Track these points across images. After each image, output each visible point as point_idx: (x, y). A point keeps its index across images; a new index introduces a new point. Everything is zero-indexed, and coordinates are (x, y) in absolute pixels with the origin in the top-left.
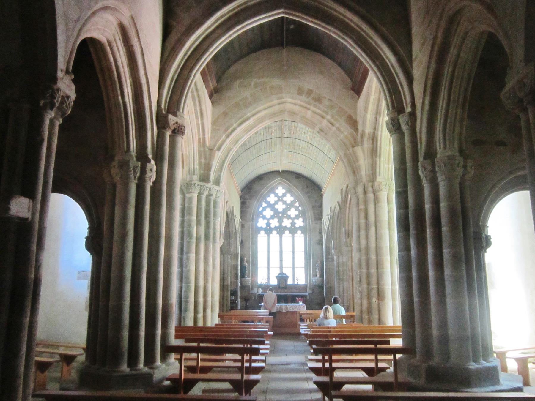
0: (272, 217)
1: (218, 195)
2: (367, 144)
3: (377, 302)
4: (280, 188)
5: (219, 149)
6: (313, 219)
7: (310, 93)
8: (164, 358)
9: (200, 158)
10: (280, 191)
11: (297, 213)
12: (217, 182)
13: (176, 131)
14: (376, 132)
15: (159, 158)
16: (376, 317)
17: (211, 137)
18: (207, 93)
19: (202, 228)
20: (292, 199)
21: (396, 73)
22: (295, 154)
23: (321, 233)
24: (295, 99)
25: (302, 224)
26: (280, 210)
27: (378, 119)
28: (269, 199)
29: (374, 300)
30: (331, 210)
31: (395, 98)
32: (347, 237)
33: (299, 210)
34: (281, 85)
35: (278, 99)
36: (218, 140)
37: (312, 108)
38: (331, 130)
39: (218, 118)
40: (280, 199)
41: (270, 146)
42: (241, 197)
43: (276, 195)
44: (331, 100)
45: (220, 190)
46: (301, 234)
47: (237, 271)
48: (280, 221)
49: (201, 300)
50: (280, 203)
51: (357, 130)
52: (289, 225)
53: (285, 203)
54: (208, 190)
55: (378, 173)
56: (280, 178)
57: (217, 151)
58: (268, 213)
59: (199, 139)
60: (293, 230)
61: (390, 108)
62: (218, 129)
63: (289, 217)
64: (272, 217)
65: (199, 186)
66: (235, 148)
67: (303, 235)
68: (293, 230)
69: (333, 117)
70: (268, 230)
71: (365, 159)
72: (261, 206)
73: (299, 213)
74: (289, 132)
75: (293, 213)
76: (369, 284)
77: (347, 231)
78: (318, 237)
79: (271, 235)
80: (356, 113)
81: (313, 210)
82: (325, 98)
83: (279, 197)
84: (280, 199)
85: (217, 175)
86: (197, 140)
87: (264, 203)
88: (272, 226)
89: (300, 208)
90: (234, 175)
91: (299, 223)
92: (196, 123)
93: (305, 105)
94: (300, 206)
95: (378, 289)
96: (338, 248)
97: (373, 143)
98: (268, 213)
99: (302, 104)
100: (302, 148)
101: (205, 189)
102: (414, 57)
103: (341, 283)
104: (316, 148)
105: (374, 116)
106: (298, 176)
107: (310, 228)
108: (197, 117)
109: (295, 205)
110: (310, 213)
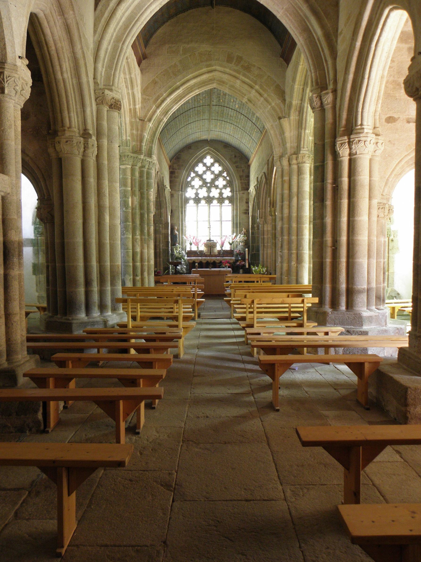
0: (201, 187)
1: (151, 166)
2: (294, 116)
3: (295, 265)
4: (208, 157)
5: (150, 120)
6: (240, 189)
7: (240, 59)
8: (114, 310)
9: (132, 129)
10: (208, 160)
11: (224, 183)
12: (150, 155)
13: (113, 106)
14: (303, 103)
15: (99, 134)
16: (294, 278)
17: (142, 108)
18: (135, 60)
19: (137, 199)
20: (220, 169)
21: (322, 48)
22: (223, 122)
23: (247, 203)
24: (225, 67)
25: (230, 194)
26: (209, 180)
27: (305, 89)
28: (197, 169)
29: (294, 263)
30: (257, 181)
31: (319, 73)
32: (271, 207)
35: (208, 66)
37: (241, 77)
39: (147, 88)
41: (198, 114)
42: (170, 167)
44: (260, 68)
47: (168, 239)
48: (209, 191)
49: (138, 264)
50: (208, 173)
51: (284, 100)
52: (217, 196)
53: (213, 173)
54: (140, 162)
55: (302, 146)
57: (148, 123)
58: (197, 183)
59: (130, 109)
60: (221, 200)
61: (314, 84)
63: (217, 187)
64: (201, 187)
65: (132, 158)
66: (165, 119)
67: (230, 204)
68: (221, 200)
69: (261, 87)
70: (197, 200)
71: (290, 131)
72: (190, 176)
73: (228, 183)
74: (218, 99)
75: (221, 182)
76: (289, 249)
77: (272, 201)
78: (244, 207)
79: (199, 205)
80: (284, 83)
81: (241, 180)
83: (207, 167)
84: (208, 168)
86: (128, 110)
87: (192, 173)
89: (228, 178)
90: (163, 144)
91: (227, 193)
92: (126, 93)
94: (227, 176)
95: (297, 254)
96: (264, 217)
97: (299, 115)
98: (197, 183)
102: (339, 31)
103: (265, 249)
104: (244, 117)
105: (302, 87)
106: (227, 145)
108: (127, 87)
109: (223, 175)
110: (237, 183)
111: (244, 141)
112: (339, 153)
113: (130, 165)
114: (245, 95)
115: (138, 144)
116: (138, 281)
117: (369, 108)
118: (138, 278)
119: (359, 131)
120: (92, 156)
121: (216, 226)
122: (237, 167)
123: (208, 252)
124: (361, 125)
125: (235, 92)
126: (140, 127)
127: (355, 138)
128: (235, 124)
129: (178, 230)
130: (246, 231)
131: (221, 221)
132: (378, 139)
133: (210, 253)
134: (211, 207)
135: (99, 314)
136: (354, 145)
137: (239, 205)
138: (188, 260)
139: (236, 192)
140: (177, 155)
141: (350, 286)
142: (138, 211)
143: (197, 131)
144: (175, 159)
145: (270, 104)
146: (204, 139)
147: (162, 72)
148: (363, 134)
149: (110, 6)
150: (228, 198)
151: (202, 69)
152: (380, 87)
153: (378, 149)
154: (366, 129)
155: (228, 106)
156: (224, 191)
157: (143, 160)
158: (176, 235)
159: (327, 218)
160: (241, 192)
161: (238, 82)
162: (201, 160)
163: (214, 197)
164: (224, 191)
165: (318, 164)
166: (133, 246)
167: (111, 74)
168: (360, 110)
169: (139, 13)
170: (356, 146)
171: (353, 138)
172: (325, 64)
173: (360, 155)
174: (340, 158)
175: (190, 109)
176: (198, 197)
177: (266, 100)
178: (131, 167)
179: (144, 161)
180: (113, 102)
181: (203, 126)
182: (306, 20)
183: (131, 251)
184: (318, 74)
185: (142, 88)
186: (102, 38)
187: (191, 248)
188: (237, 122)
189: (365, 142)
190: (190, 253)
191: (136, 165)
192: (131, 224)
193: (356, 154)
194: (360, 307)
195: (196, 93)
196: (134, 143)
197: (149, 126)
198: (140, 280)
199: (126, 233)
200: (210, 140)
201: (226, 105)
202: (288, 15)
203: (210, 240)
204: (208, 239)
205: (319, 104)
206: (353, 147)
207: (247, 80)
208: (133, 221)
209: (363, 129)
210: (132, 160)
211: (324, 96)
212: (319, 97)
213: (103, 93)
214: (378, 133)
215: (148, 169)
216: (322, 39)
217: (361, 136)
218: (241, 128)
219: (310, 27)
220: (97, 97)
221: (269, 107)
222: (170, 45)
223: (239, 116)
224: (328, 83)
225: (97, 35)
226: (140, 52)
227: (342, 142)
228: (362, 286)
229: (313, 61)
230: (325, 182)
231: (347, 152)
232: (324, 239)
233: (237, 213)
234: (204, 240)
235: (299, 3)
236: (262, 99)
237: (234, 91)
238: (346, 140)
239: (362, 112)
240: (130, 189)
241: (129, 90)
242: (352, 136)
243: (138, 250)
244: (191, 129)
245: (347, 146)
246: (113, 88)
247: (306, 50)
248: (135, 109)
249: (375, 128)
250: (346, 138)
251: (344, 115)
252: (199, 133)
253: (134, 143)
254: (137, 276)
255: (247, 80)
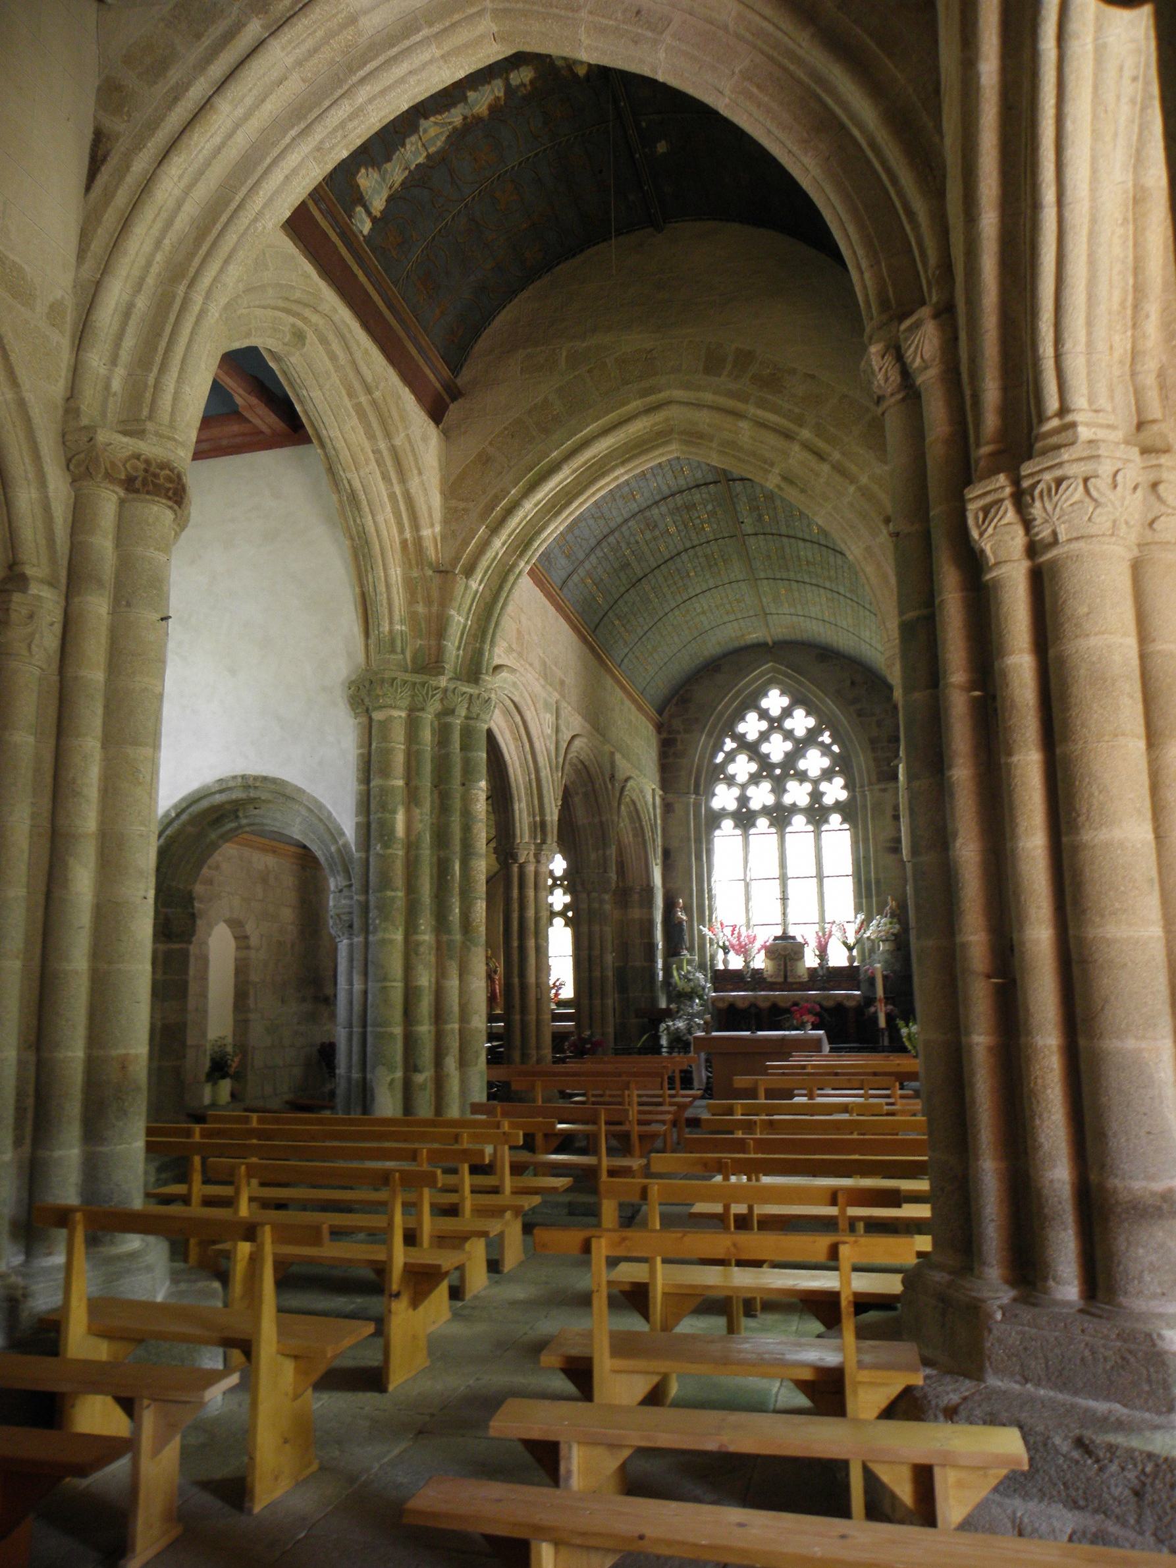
0: (755, 779)
1: (476, 710)
4: (774, 693)
5: (469, 572)
6: (874, 778)
7: (744, 359)
9: (412, 600)
10: (775, 701)
11: (826, 762)
13: (138, 484)
17: (444, 537)
19: (425, 814)
20: (811, 722)
22: (794, 585)
25: (843, 795)
28: (741, 728)
33: (833, 752)
34: (651, 351)
35: (644, 393)
36: (466, 543)
37: (752, 410)
38: (817, 475)
39: (462, 477)
40: (776, 725)
43: (764, 714)
44: (813, 377)
45: (479, 695)
46: (841, 824)
48: (779, 788)
49: (425, 1029)
50: (776, 738)
52: (803, 801)
53: (788, 735)
54: (438, 697)
56: (771, 664)
58: (742, 767)
59: (404, 543)
60: (817, 813)
62: (463, 510)
63: (802, 777)
64: (755, 779)
68: (817, 813)
69: (819, 431)
70: (744, 818)
74: (755, 514)
75: (814, 762)
81: (874, 750)
82: (793, 372)
83: (771, 720)
84: (776, 724)
85: (470, 648)
87: (728, 740)
88: (755, 805)
89: (836, 749)
91: (835, 791)
93: (731, 403)
98: (742, 767)
99: (723, 401)
100: (808, 562)
101: (427, 694)
106: (825, 654)
107: (864, 806)
108: (385, 477)
109: (820, 739)
110: (862, 761)
111: (866, 634)
112: (982, 551)
113: (400, 709)
114: (772, 465)
115: (433, 643)
116: (423, 1087)
117: (1089, 334)
118: (424, 1077)
119: (1054, 440)
120: (25, 653)
121: (803, 894)
122: (860, 713)
123: (778, 976)
124: (1063, 410)
125: (740, 460)
126: (435, 594)
127: (1041, 471)
128: (828, 585)
129: (687, 909)
130: (898, 906)
131: (820, 877)
132: (1159, 466)
133: (786, 977)
134: (788, 837)
135: (21, 1258)
136: (1038, 504)
137: (874, 827)
138: (715, 1000)
139: (862, 786)
140: (681, 692)
141: (1093, 1177)
142: (426, 853)
143: (726, 619)
144: (677, 704)
145: (852, 480)
146: (755, 641)
147: (506, 429)
148: (1072, 449)
149: (134, 169)
150: (838, 807)
151: (628, 403)
152: (1136, 245)
153: (1163, 509)
154: (1087, 425)
155: (791, 533)
156: (824, 786)
157: (445, 690)
158: (680, 923)
159: (959, 842)
160: (877, 787)
161: (744, 425)
162: (751, 702)
163: (794, 805)
164: (824, 786)
165: (911, 615)
166: (408, 969)
167: (146, 385)
168: (1047, 349)
169: (243, 184)
170: (1049, 507)
171: (1032, 475)
172: (908, 228)
173: (1075, 546)
174: (990, 569)
175: (679, 554)
176: (749, 810)
177: (838, 469)
178: (409, 716)
179: (449, 693)
180: (135, 468)
181: (738, 601)
182: (819, 91)
183: (399, 985)
184: (884, 270)
185: (444, 480)
186: (106, 268)
187: (725, 962)
188: (829, 578)
189: (1086, 480)
190: (724, 979)
191: (423, 709)
192: (400, 894)
193: (1055, 542)
194: (1154, 1296)
195: (617, 478)
196: (419, 642)
197: (467, 587)
198: (430, 1086)
199: (383, 925)
200: (774, 643)
201: (784, 530)
202: (755, 90)
203: (785, 937)
204: (779, 933)
205: (895, 377)
206: (1037, 510)
207: (772, 418)
208: (411, 887)
209: (1073, 425)
210: (407, 693)
211: (906, 339)
212: (893, 351)
213: (91, 439)
214: (1159, 444)
215: (467, 718)
216: (883, 137)
217: (1066, 457)
218: (848, 595)
219: (838, 111)
220: (70, 456)
221: (852, 489)
222: (529, 350)
223: (832, 559)
224: (926, 294)
225: (89, 263)
226: (432, 377)
227: (988, 499)
228: (1151, 1178)
229: (861, 226)
230: (942, 683)
231: (1017, 540)
232: (959, 939)
233: (867, 850)
234: (766, 935)
235: (786, 39)
236: (825, 468)
237: (734, 456)
238: (1003, 488)
239: (1058, 357)
240: (400, 783)
241: (392, 484)
242: (1026, 469)
243: (425, 979)
244: (704, 613)
245: (1011, 515)
246: (150, 426)
247: (832, 197)
248: (418, 541)
249: (1140, 426)
250: (1002, 479)
251: (991, 392)
252: (735, 624)
253: (419, 642)
254: (416, 1069)
255: (772, 418)
